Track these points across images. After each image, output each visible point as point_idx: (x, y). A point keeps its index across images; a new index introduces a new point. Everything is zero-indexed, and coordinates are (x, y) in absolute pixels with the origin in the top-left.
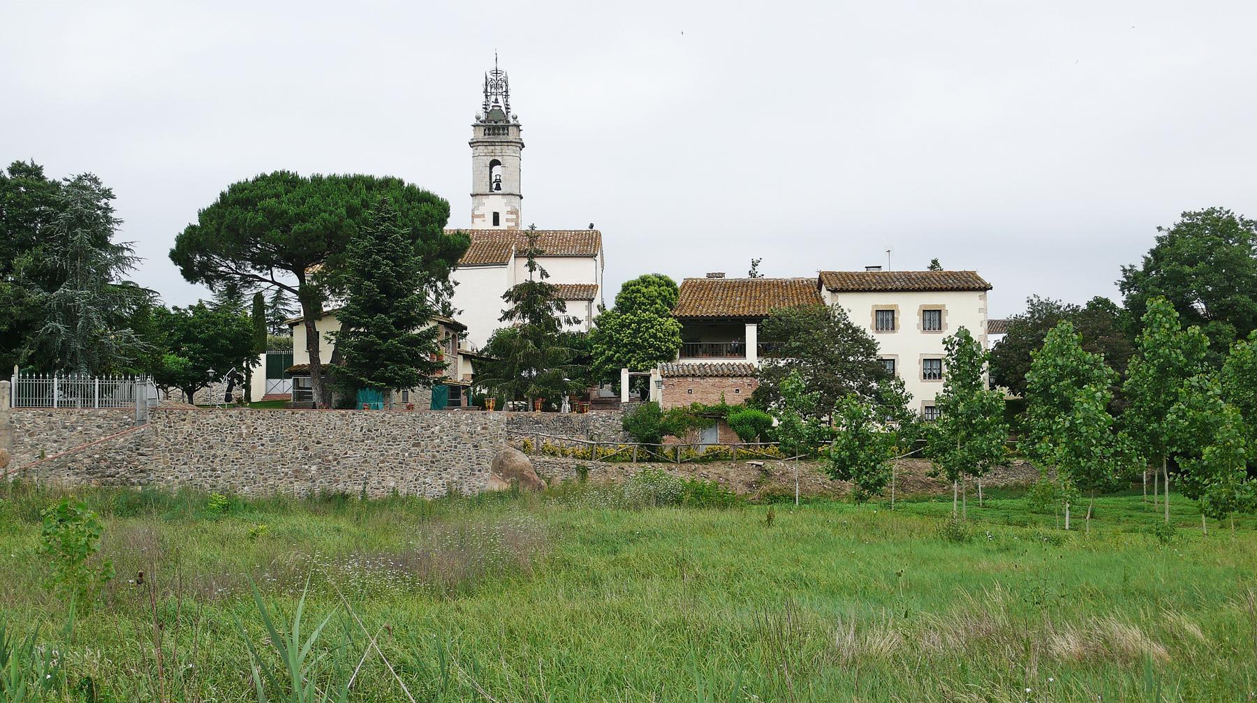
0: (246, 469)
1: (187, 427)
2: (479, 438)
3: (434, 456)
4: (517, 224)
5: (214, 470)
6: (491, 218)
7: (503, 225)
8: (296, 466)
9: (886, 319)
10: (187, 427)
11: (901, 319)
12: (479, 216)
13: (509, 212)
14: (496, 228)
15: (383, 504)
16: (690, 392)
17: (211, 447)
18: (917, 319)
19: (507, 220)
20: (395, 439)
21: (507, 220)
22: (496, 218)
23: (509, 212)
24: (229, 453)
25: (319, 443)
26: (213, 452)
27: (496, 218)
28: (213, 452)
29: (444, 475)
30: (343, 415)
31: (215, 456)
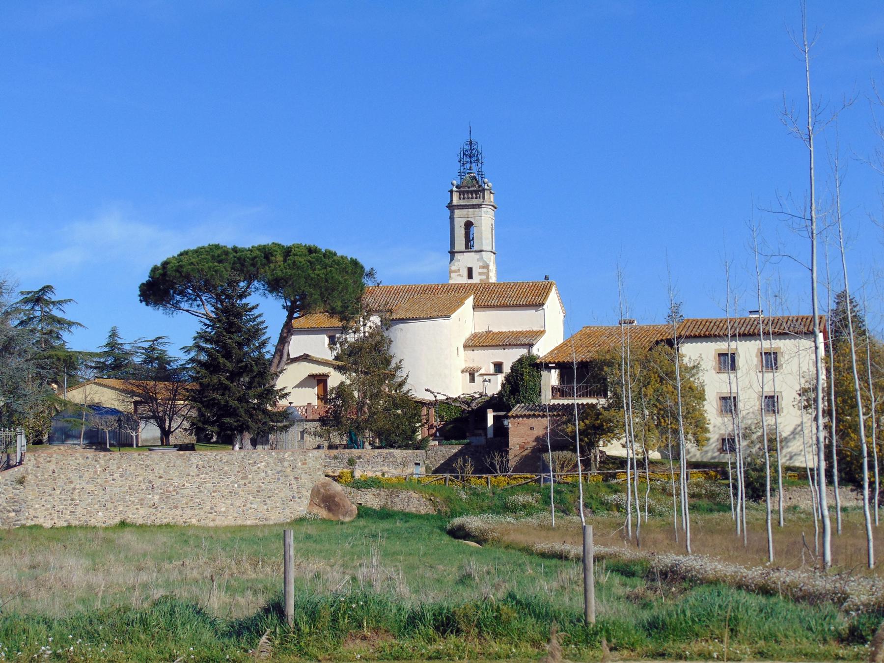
0: (100, 499)
1: (52, 466)
2: (300, 471)
3: (260, 487)
4: (488, 278)
5: (72, 500)
6: (465, 273)
7: (476, 279)
8: (142, 496)
9: (728, 362)
10: (52, 466)
11: (741, 362)
12: (455, 271)
13: (481, 267)
14: (470, 281)
15: (160, 526)
16: (532, 429)
17: (71, 482)
18: (755, 361)
19: (480, 274)
20: (226, 473)
21: (480, 274)
22: (470, 271)
23: (481, 267)
24: (86, 486)
25: (160, 477)
26: (72, 486)
27: (470, 271)
28: (72, 486)
29: (268, 502)
30: (181, 455)
31: (74, 489)
